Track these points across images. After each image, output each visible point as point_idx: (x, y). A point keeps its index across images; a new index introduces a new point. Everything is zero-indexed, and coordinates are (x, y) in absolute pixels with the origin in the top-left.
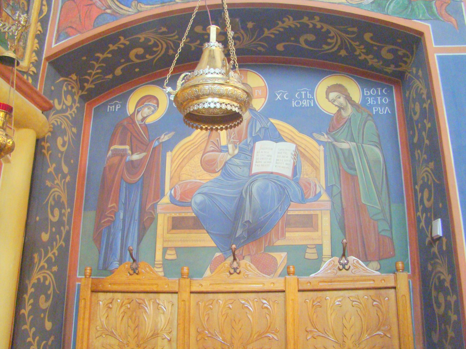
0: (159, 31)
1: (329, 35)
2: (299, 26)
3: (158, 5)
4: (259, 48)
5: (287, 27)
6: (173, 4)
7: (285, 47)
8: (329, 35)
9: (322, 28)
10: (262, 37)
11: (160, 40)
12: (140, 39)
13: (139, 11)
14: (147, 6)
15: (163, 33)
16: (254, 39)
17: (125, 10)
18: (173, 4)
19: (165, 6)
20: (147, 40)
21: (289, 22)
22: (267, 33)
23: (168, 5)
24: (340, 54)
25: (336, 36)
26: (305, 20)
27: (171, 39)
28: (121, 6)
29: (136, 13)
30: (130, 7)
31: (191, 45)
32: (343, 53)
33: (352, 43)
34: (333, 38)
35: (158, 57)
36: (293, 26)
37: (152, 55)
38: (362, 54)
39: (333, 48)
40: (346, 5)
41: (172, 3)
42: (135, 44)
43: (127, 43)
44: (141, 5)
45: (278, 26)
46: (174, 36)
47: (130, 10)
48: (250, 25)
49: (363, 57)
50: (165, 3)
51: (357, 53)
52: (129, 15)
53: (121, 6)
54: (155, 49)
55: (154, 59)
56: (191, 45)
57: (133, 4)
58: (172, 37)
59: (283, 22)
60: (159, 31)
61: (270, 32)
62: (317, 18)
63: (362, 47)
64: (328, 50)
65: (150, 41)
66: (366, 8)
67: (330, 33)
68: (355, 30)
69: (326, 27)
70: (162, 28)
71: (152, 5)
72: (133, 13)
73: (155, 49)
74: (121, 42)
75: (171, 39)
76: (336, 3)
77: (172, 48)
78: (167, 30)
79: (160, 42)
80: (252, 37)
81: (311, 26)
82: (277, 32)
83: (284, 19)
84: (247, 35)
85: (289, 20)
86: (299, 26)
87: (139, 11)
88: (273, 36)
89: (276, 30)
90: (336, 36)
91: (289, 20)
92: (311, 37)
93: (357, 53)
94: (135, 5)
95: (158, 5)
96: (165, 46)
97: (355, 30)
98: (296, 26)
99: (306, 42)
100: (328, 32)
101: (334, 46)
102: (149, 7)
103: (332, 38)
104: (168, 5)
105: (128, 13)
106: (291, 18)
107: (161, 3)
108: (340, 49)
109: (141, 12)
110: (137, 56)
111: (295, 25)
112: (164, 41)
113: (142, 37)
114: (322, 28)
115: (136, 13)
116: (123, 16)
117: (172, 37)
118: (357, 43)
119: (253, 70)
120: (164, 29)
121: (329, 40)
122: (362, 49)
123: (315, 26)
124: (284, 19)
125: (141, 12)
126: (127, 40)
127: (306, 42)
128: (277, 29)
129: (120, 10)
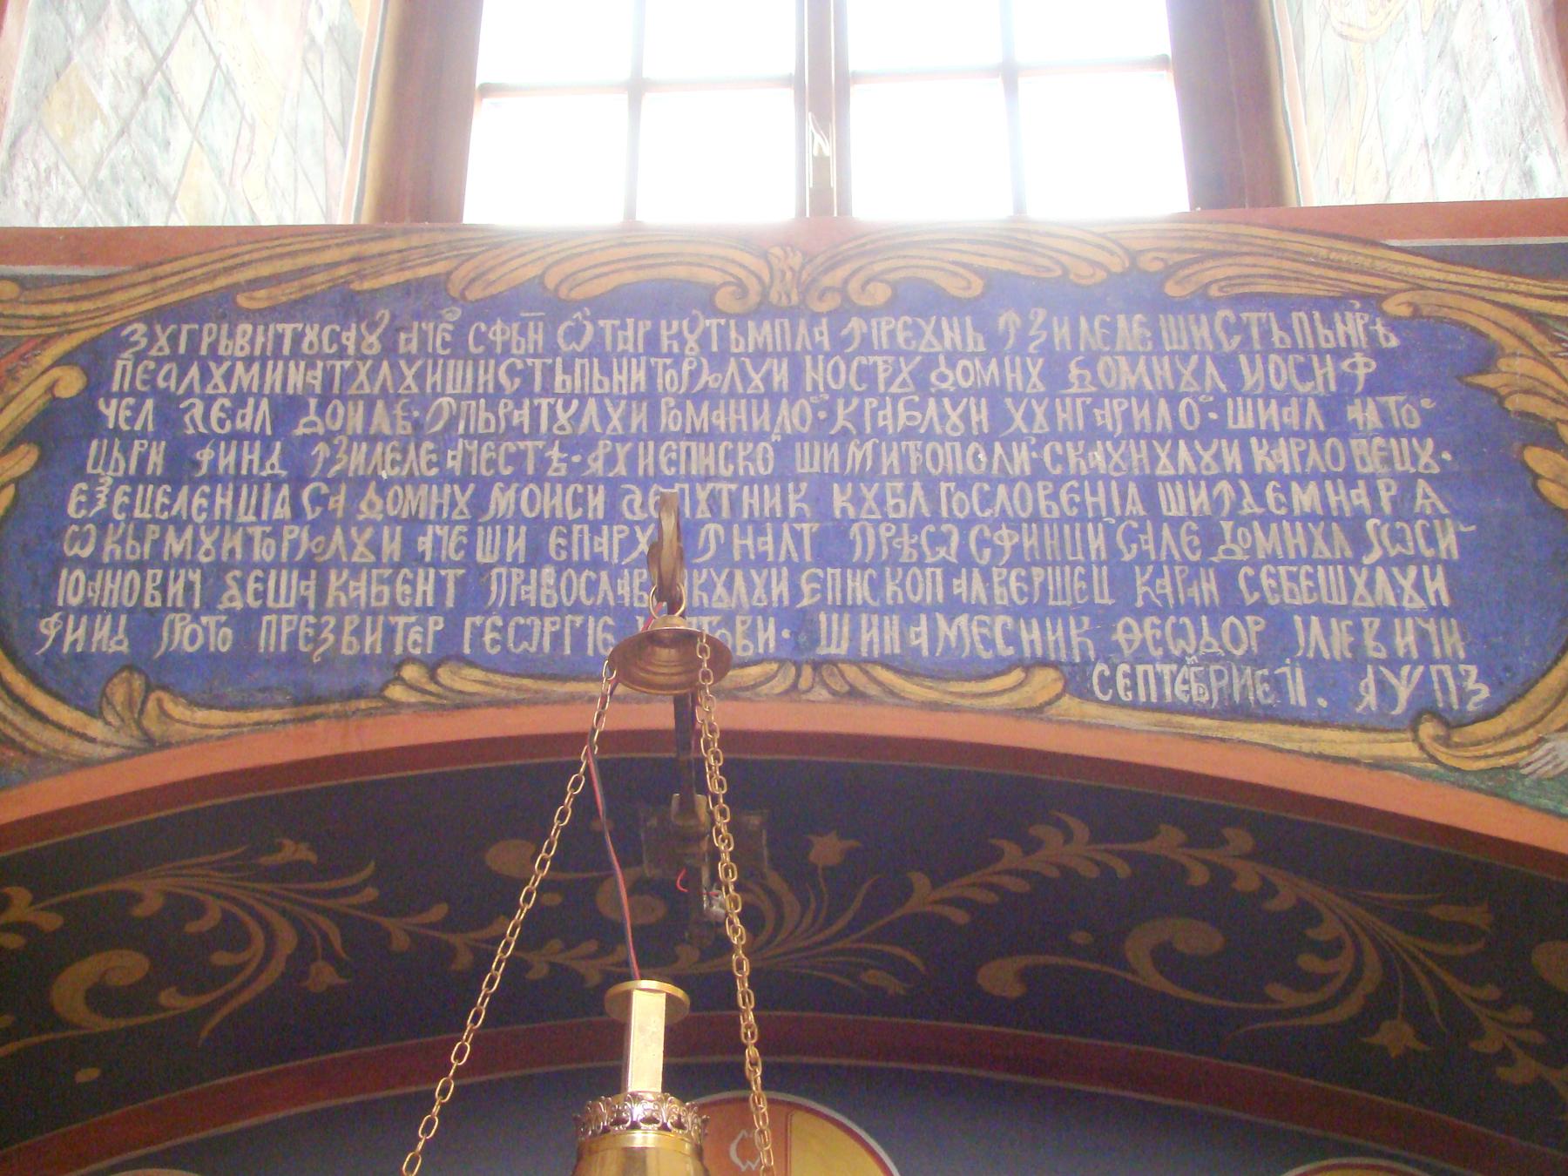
0: (266, 860)
1: (1311, 933)
2: (1123, 870)
3: (277, 715)
4: (873, 977)
5: (1054, 873)
6: (368, 713)
7: (1024, 975)
8: (1311, 933)
9: (1268, 890)
10: (898, 913)
11: (260, 907)
12: (134, 898)
13: (151, 744)
14: (201, 715)
15: (296, 870)
16: (840, 924)
17: (60, 727)
18: (368, 713)
19: (320, 723)
20: (183, 907)
21: (1068, 849)
22: (923, 894)
23: (339, 716)
24: (1380, 1038)
25: (1358, 948)
26: (1168, 841)
27: (330, 903)
28: (40, 700)
29: (130, 753)
30: (94, 713)
31: (456, 940)
32: (1395, 1036)
33: (1459, 988)
34: (1328, 950)
35: (234, 1004)
36: (1090, 872)
37: (200, 991)
38: (1519, 1054)
39: (1323, 1006)
40: (1422, 775)
41: (363, 704)
42: (100, 927)
43: (51, 921)
44: (169, 706)
45: (999, 867)
46: (356, 889)
47: (96, 729)
48: (827, 849)
49: (1522, 1071)
50: (319, 701)
51: (1488, 1044)
52: (84, 764)
53: (40, 700)
54: (222, 958)
55: (209, 1010)
56: (456, 940)
57: (118, 693)
58: (345, 892)
59: (1031, 846)
60: (266, 860)
61: (946, 892)
62: (1240, 840)
63: (1520, 1013)
64: (1299, 1012)
65: (198, 910)
66: (1544, 802)
67: (1317, 920)
68: (1478, 916)
69: (1288, 892)
70: (288, 843)
71: (242, 707)
72: (110, 752)
73: (222, 958)
74: (12, 915)
75: (330, 903)
76: (1355, 762)
77: (331, 957)
78: (312, 857)
79: (259, 918)
80: (829, 921)
81: (1199, 876)
82: (990, 897)
83: (1039, 831)
84: (805, 907)
85: (1069, 837)
86: (1123, 870)
87: (151, 744)
88: (960, 917)
89: (992, 887)
90: (1358, 948)
91: (1069, 837)
92: (1198, 938)
93: (1488, 1044)
94: (130, 703)
95: (277, 715)
96: (287, 940)
97: (1478, 916)
98: (1107, 870)
99: (1165, 957)
100: (1306, 913)
101: (1345, 991)
102: (217, 716)
103: (1328, 950)
104: (339, 716)
105: (77, 746)
106: (1080, 830)
107: (297, 703)
108: (1376, 1011)
109: (167, 745)
110: (100, 997)
111: (1097, 863)
112: (284, 913)
113: (150, 893)
114: (1268, 890)
115: (130, 753)
116: (42, 762)
117: (345, 892)
118: (1490, 992)
119: (814, 1096)
120: (294, 851)
121: (1309, 962)
122: (1519, 1026)
123: (1223, 878)
124: (1039, 831)
125: (167, 745)
126: (52, 908)
127: (1165, 957)
128: (995, 879)
129: (33, 727)
